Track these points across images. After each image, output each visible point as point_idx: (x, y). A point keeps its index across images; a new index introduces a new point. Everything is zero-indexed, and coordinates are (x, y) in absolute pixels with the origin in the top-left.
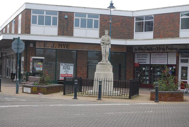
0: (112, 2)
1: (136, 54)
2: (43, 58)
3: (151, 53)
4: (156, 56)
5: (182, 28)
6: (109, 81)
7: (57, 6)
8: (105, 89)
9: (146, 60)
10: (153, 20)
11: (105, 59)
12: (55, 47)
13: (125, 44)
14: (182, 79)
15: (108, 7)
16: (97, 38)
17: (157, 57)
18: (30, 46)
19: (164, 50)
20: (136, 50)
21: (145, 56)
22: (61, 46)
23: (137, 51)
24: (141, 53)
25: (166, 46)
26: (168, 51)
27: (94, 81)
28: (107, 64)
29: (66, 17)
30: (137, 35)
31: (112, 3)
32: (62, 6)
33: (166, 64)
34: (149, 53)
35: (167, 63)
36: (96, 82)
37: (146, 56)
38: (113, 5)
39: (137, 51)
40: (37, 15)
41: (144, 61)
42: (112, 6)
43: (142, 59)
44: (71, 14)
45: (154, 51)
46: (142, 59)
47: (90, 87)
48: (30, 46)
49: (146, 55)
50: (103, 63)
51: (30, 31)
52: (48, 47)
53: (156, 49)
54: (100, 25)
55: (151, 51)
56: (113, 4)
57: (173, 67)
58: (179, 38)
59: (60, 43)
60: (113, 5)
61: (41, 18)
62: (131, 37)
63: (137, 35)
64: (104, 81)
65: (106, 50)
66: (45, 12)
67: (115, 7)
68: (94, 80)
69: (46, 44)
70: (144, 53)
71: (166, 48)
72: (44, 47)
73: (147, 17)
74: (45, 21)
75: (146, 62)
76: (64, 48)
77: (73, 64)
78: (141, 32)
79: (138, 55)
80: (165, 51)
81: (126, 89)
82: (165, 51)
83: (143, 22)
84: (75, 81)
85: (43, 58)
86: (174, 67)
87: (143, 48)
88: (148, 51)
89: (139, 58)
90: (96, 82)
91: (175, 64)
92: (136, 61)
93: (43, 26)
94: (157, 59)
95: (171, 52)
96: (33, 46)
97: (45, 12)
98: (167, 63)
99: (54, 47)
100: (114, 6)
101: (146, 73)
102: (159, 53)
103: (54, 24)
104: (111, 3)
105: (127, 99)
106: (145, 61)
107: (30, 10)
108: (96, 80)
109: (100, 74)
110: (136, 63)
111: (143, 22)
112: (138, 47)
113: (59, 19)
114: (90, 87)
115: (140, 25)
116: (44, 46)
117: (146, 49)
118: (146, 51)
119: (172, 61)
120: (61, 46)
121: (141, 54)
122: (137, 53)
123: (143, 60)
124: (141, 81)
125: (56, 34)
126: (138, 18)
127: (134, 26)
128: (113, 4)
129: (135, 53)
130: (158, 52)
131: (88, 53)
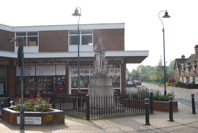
0: (166, 11)
4: (43, 68)
6: (111, 97)
9: (30, 72)
15: (163, 16)
19: (52, 62)
25: (54, 59)
26: (56, 63)
31: (167, 12)
33: (54, 75)
35: (36, 75)
38: (168, 14)
41: (28, 73)
45: (40, 64)
47: (101, 107)
49: (30, 67)
55: (36, 64)
56: (168, 13)
57: (17, 75)
58: (67, 52)
60: (168, 14)
62: (66, 50)
64: (109, 98)
75: (30, 74)
77: (3, 84)
83: (26, 37)
86: (63, 78)
87: (26, 61)
88: (32, 64)
91: (65, 74)
95: (51, 65)
102: (46, 66)
104: (166, 12)
106: (29, 73)
111: (26, 37)
114: (101, 107)
118: (30, 64)
119: (61, 72)
126: (19, 34)
128: (168, 13)
130: (45, 65)
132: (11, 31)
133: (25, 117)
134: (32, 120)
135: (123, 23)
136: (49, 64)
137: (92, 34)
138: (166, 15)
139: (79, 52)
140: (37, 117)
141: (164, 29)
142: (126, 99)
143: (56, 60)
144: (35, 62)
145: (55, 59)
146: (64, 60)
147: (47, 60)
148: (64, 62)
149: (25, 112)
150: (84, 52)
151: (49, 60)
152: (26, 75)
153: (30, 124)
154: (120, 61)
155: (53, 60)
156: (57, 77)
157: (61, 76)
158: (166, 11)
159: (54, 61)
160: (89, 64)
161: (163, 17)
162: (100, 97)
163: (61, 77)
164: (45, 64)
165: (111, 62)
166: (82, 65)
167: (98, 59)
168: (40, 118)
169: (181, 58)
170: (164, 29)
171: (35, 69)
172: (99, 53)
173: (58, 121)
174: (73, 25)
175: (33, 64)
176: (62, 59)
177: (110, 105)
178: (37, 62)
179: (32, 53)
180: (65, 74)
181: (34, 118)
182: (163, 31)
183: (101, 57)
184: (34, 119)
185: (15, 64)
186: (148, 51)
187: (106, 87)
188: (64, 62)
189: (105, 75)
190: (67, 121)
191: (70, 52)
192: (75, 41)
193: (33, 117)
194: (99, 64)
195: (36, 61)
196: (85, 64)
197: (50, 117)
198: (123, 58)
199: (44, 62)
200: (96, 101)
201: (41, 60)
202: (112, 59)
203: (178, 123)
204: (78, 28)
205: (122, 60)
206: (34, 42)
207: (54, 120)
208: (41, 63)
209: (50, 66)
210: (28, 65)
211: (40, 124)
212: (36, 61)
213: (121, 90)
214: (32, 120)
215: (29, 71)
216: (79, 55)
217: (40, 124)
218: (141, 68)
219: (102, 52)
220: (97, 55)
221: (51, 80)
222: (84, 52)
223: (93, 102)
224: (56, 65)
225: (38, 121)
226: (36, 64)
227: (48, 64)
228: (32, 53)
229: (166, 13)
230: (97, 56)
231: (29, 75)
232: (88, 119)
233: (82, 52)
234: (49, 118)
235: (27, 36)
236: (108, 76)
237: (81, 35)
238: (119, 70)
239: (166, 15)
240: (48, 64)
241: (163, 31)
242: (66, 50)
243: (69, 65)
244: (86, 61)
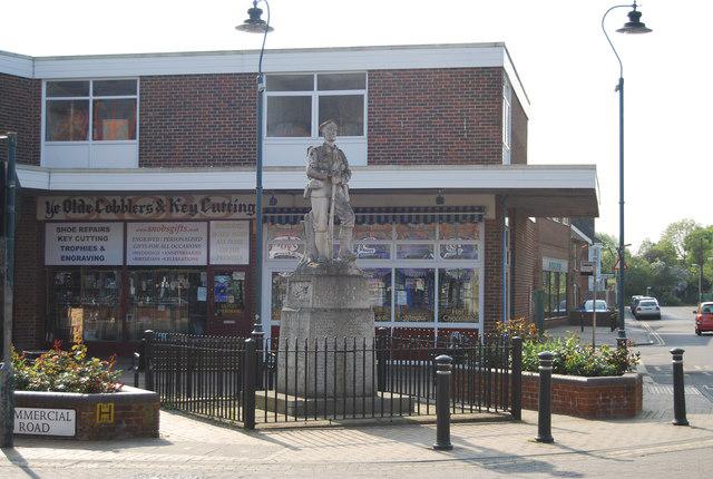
0: (635, 6)
1: (51, 230)
3: (125, 222)
5: (271, 132)
9: (102, 249)
13: (44, 186)
14: (433, 320)
15: (622, 26)
16: (129, 170)
17: (158, 239)
19: (194, 210)
26: (210, 214)
30: (50, 150)
33: (203, 262)
34: (117, 221)
35: (208, 260)
37: (105, 234)
38: (642, 20)
39: (61, 215)
42: (255, 21)
45: (144, 215)
47: (321, 387)
49: (103, 229)
53: (155, 206)
56: (639, 14)
58: (522, 166)
60: (642, 20)
62: (249, 156)
67: (647, 26)
70: (93, 221)
71: (65, 205)
78: (81, 142)
80: (197, 216)
81: (359, 384)
82: (197, 216)
83: (88, 101)
86: (239, 276)
87: (87, 201)
88: (112, 216)
91: (245, 261)
92: (53, 257)
94: (157, 246)
95: (187, 221)
98: (208, 260)
100: (643, 25)
101: (232, 301)
102: (167, 224)
104: (632, 9)
112: (63, 199)
114: (321, 387)
118: (104, 215)
119: (229, 249)
121: (78, 225)
122: (56, 221)
126: (61, 87)
128: (639, 14)
132: (28, 75)
133: (17, 410)
134: (43, 421)
135: (496, 45)
136: (180, 215)
137: (364, 92)
138: (635, 23)
140: (60, 411)
141: (622, 80)
142: (493, 370)
143: (209, 200)
144: (123, 207)
145: (207, 195)
146: (242, 200)
147: (171, 200)
148: (242, 208)
149: (16, 392)
151: (183, 201)
152: (87, 263)
153: (37, 433)
154: (481, 209)
155: (197, 201)
156: (213, 270)
157: (227, 270)
158: (635, 6)
159: (203, 203)
160: (457, 217)
161: (622, 31)
163: (230, 274)
164: (163, 216)
165: (433, 210)
166: (363, 222)
167: (319, 204)
168: (72, 413)
170: (622, 80)
171: (122, 231)
172: (321, 184)
173: (134, 426)
174: (282, 51)
175: (116, 218)
176: (234, 197)
177: (291, 377)
178: (131, 208)
180: (245, 261)
181: (52, 413)
182: (620, 87)
183: (330, 199)
184: (52, 416)
185: (41, 214)
186: (593, 168)
187: (342, 313)
188: (242, 208)
189: (343, 266)
190: (169, 423)
192: (294, 120)
193: (47, 411)
194: (321, 224)
195: (126, 203)
196: (422, 218)
197: (107, 410)
198: (493, 196)
199: (161, 208)
200: (301, 364)
201: (141, 202)
202: (440, 200)
203: (565, 447)
205: (490, 203)
206: (121, 124)
207: (118, 422)
208: (149, 209)
209: (185, 224)
211: (72, 432)
212: (126, 203)
213: (481, 333)
214: (43, 421)
215: (99, 244)
217: (72, 432)
218: (683, 234)
219: (336, 180)
220: (315, 189)
221: (598, 306)
223: (291, 371)
224: (208, 220)
225: (64, 422)
226: (127, 216)
227: (175, 215)
228: (107, 171)
229: (255, 13)
230: (314, 193)
231: (96, 263)
232: (249, 426)
234: (101, 413)
235: (91, 98)
236: (356, 272)
237: (315, 95)
238: (469, 248)
239: (635, 23)
240: (175, 215)
241: (620, 87)
242: (249, 156)
243: (265, 220)
244: (393, 204)
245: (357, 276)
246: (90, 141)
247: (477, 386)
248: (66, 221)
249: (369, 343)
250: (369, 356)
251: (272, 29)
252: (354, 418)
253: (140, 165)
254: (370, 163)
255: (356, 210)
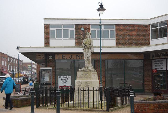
0: (101, 3)
1: (153, 61)
2: (51, 68)
3: (166, 58)
6: (83, 91)
7: (73, 19)
8: (87, 99)
10: (167, 26)
11: (90, 66)
12: (73, 58)
18: (49, 58)
20: (153, 57)
21: (160, 62)
22: (79, 57)
23: (154, 58)
24: (158, 59)
27: (75, 91)
28: (89, 70)
29: (83, 29)
30: (153, 42)
32: (78, 19)
36: (77, 91)
37: (162, 62)
38: (103, 7)
39: (154, 58)
40: (55, 29)
42: (101, 8)
43: (159, 65)
44: (87, 27)
46: (159, 65)
48: (49, 58)
50: (85, 69)
51: (49, 44)
52: (66, 58)
54: (116, 35)
56: (103, 5)
59: (77, 54)
60: (103, 7)
61: (59, 31)
62: (147, 44)
63: (153, 42)
64: (94, 91)
65: (87, 55)
66: (62, 26)
67: (105, 8)
68: (75, 90)
69: (63, 56)
72: (63, 58)
73: (162, 23)
74: (63, 34)
76: (82, 58)
78: (157, 39)
79: (155, 61)
83: (158, 28)
84: (57, 92)
85: (51, 68)
87: (159, 54)
88: (163, 57)
89: (156, 65)
90: (77, 91)
92: (154, 68)
93: (61, 39)
96: (52, 58)
97: (62, 26)
99: (72, 58)
100: (104, 8)
103: (72, 36)
104: (100, 4)
105: (104, 111)
106: (162, 67)
107: (49, 25)
108: (77, 89)
109: (81, 82)
110: (153, 70)
111: (158, 28)
113: (76, 31)
115: (155, 31)
116: (63, 57)
117: (162, 55)
120: (79, 57)
121: (158, 60)
123: (160, 66)
124: (159, 87)
125: (74, 45)
126: (153, 26)
127: (152, 35)
129: (152, 60)
131: (105, 62)
139: (101, 47)
150: (105, 47)
155: (154, 54)
162: (87, 90)
169: (15, 54)
179: (57, 47)
191: (52, 47)
204: (100, 23)
210: (160, 58)
215: (162, 64)
216: (101, 50)
222: (105, 47)
229: (101, 6)
233: (103, 47)
245: (124, 72)
246: (159, 38)
247: (42, 101)
248: (156, 59)
249: (98, 89)
250: (98, 92)
251: (97, 10)
252: (66, 107)
253: (116, 46)
254: (117, 46)
255: (84, 60)
